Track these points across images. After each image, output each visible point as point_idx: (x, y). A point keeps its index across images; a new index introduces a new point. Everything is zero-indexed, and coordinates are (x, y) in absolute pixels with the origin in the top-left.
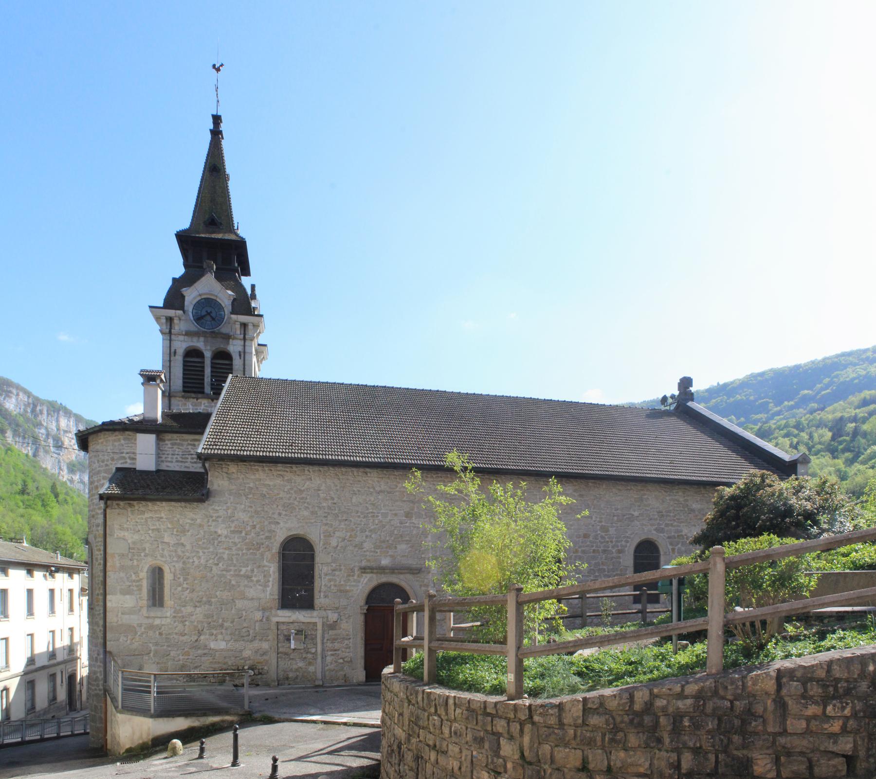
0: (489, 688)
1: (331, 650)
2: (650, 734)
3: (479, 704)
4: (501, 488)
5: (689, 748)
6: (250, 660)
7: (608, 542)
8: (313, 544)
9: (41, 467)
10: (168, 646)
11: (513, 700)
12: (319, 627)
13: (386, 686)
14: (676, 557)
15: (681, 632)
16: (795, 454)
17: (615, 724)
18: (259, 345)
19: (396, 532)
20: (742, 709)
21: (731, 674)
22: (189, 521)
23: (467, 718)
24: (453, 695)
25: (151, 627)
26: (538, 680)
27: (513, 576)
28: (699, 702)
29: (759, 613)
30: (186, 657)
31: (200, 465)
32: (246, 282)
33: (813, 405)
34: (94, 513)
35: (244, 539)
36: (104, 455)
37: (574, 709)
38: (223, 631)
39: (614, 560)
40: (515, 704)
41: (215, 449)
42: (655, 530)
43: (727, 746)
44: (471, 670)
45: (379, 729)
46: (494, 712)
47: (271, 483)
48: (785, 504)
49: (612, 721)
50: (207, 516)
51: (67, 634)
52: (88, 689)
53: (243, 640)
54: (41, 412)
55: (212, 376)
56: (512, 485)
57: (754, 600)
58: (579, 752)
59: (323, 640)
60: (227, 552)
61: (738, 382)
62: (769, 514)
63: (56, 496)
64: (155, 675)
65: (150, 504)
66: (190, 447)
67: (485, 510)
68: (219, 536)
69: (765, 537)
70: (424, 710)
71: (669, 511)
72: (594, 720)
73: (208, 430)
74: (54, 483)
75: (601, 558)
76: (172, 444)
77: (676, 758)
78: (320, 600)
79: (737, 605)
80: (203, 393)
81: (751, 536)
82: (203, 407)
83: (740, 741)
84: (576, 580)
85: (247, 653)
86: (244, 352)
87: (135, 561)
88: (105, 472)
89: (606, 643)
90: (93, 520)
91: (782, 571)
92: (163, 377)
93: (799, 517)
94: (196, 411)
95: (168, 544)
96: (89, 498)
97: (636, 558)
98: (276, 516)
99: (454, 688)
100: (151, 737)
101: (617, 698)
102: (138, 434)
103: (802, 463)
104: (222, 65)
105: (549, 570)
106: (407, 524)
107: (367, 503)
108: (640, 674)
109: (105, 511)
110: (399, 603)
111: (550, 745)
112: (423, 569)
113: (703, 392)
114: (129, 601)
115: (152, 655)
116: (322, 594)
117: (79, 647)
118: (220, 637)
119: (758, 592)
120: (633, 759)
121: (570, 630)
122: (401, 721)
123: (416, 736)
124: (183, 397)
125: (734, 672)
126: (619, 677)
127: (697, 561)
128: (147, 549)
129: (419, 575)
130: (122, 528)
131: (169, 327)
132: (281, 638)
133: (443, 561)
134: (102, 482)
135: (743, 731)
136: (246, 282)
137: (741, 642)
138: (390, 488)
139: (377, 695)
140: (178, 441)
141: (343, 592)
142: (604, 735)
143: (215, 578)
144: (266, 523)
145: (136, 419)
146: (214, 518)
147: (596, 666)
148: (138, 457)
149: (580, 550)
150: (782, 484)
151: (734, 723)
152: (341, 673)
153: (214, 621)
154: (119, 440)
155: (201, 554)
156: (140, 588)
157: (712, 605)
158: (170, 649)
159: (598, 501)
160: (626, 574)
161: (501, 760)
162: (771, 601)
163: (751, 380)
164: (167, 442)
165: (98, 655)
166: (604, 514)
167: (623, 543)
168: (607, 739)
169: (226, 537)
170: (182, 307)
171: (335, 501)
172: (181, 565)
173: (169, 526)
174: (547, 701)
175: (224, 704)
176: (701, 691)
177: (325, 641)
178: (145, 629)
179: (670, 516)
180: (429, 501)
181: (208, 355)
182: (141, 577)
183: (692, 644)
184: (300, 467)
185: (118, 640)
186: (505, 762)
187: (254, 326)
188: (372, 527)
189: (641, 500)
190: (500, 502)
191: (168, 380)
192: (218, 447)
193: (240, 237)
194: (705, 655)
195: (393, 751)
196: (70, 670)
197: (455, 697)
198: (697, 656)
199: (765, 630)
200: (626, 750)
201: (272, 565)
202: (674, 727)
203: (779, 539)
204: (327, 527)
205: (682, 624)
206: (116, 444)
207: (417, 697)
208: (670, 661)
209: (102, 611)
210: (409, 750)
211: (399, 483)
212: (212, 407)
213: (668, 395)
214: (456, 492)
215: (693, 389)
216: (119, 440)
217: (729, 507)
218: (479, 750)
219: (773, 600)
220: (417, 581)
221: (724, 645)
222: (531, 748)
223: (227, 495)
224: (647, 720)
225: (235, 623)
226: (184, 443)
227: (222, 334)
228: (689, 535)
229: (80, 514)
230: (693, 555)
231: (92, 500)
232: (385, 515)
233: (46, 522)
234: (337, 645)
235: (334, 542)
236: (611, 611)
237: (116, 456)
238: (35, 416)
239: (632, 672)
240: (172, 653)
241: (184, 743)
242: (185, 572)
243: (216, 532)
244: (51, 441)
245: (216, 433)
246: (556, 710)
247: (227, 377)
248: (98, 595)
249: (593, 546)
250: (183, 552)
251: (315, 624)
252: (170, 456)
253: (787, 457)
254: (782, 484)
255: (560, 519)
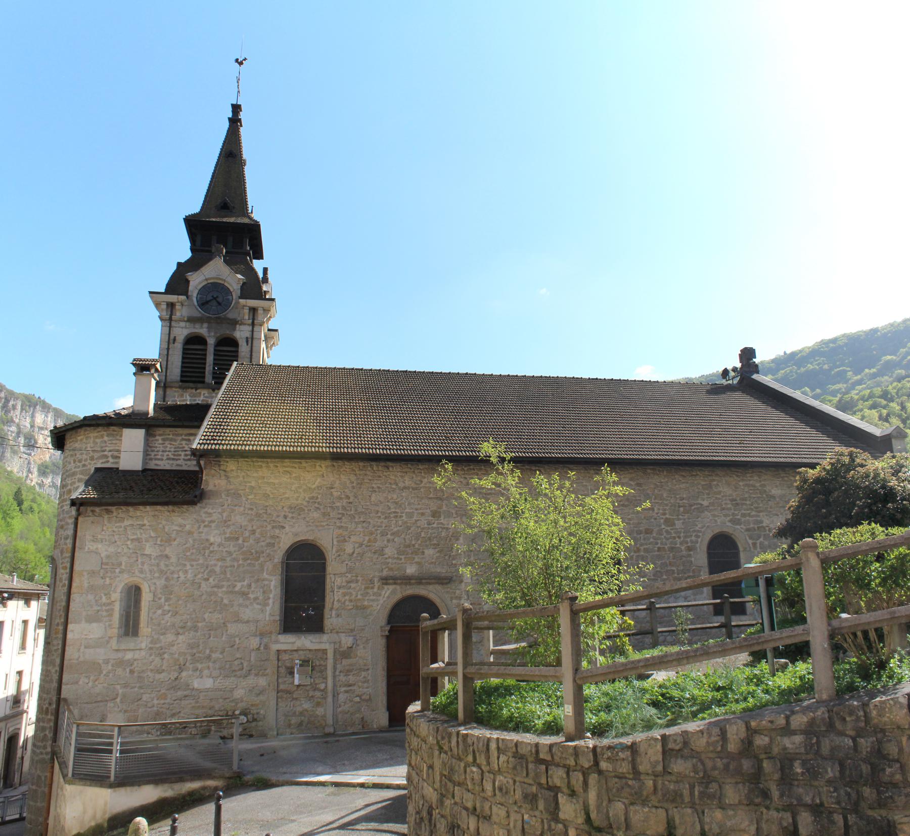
0: (541, 725)
1: (346, 686)
2: (752, 786)
3: (529, 748)
4: (545, 480)
5: (806, 805)
6: (242, 701)
7: (674, 538)
8: (324, 551)
9: (6, 471)
10: (141, 688)
11: (572, 740)
12: (330, 655)
13: (412, 730)
14: (759, 553)
15: (776, 645)
16: (887, 428)
17: (705, 772)
18: (269, 330)
19: (423, 535)
20: (869, 749)
21: (848, 700)
22: (177, 528)
23: (514, 768)
24: (495, 736)
25: (121, 663)
26: (602, 713)
27: (564, 583)
28: (811, 739)
29: (872, 619)
30: (162, 702)
31: (195, 463)
32: (258, 265)
33: (900, 371)
34: (63, 523)
35: (241, 548)
36: (82, 454)
37: (650, 752)
38: (211, 664)
39: (684, 559)
40: (575, 747)
41: (212, 444)
42: (730, 521)
43: (856, 804)
44: (517, 703)
45: (405, 792)
46: (549, 758)
47: (277, 481)
48: (884, 487)
49: (701, 767)
50: (197, 521)
51: (13, 679)
52: (33, 752)
53: (235, 676)
54: (14, 407)
55: (215, 364)
56: (558, 476)
57: (863, 604)
58: (662, 813)
59: (335, 671)
60: (220, 563)
61: (807, 351)
62: (866, 498)
63: (20, 503)
64: (120, 727)
65: (131, 509)
66: (184, 442)
67: (528, 506)
68: (211, 544)
69: (864, 527)
70: (460, 759)
71: (745, 499)
72: (679, 766)
73: (205, 423)
74: (19, 488)
75: (669, 558)
76: (163, 440)
77: (790, 820)
78: (331, 620)
79: (843, 611)
80: (203, 382)
81: (848, 526)
82: (202, 398)
83: (874, 796)
84: (640, 585)
85: (239, 693)
86: (252, 338)
87: (108, 579)
88: (82, 473)
89: (685, 661)
90: (61, 532)
91: (892, 566)
92: (158, 366)
93: (904, 502)
94: (194, 403)
95: (149, 556)
96: (59, 504)
97: (710, 555)
98: (281, 519)
99: (496, 728)
100: (107, 816)
101: (705, 734)
102: (124, 430)
103: (896, 438)
104: (245, 59)
105: (608, 573)
106: (435, 525)
107: (388, 501)
108: (732, 702)
109: (77, 519)
110: (425, 619)
111: (624, 803)
112: (455, 578)
113: (768, 363)
114: (95, 631)
115: (118, 700)
116: (334, 612)
117: (27, 698)
118: (206, 672)
119: (867, 594)
120: (734, 822)
121: (638, 650)
122: (431, 776)
123: (450, 796)
124: (180, 387)
125: (852, 697)
126: (705, 707)
127: (785, 558)
128: (124, 564)
129: (449, 585)
130: (95, 540)
131: (169, 313)
132: (282, 670)
133: (480, 567)
134: (77, 484)
135: (875, 780)
136: (258, 265)
137: (855, 660)
138: (415, 483)
139: (401, 744)
140: (171, 436)
141: (361, 609)
142: (692, 788)
143: (204, 597)
144: (269, 527)
145: (124, 412)
146: (206, 523)
147: (676, 693)
148: (122, 455)
149: (642, 548)
150: (876, 463)
151: (861, 770)
152: (357, 715)
153: (200, 653)
154: (102, 436)
155: (188, 567)
156: (110, 613)
157: (811, 609)
158: (142, 691)
159: (660, 491)
160: (701, 576)
161: (560, 826)
162: (885, 604)
163: (823, 348)
164: (157, 437)
165: (50, 704)
166: (667, 505)
167: (693, 538)
168: (696, 793)
169: (219, 545)
170: (185, 292)
171: (351, 500)
172: (163, 582)
173: (153, 534)
174: (617, 741)
175: (208, 764)
176: (812, 723)
177: (337, 673)
178: (113, 666)
179: (746, 504)
180: (461, 498)
181: (211, 341)
182: (113, 599)
183: (793, 662)
184: (311, 462)
185: (77, 683)
186: (566, 827)
187: (264, 310)
188: (395, 529)
189: (710, 487)
190: (546, 495)
191: (164, 370)
192: (216, 442)
193: (254, 220)
194: (810, 676)
195: (422, 819)
196: (11, 729)
197: (498, 739)
198: (801, 678)
199: (883, 643)
200: (723, 808)
201: (273, 578)
202: (782, 774)
203: (884, 529)
204: (341, 530)
205: (777, 634)
206: (98, 441)
207: (450, 742)
208: (767, 685)
209: (60, 647)
210: (442, 816)
211: (425, 478)
212: (212, 397)
213: (730, 368)
214: (493, 486)
215: (757, 360)
216: (102, 436)
217: (815, 492)
218: (531, 812)
219: (888, 603)
220: (448, 592)
221: (833, 663)
222: (599, 807)
223: (223, 496)
224: (747, 765)
225: (225, 654)
226: (177, 438)
227: (229, 319)
228: (772, 526)
229: (48, 526)
230: (779, 550)
231: (61, 507)
232: (410, 515)
233: (4, 538)
234: (352, 679)
235: (349, 548)
236: (688, 625)
237: (96, 455)
238: (6, 411)
239: (720, 701)
240: (145, 698)
241: (151, 822)
242: (167, 590)
243: (207, 540)
244: (22, 440)
245: (216, 426)
246: (629, 753)
247: (231, 365)
248: (58, 624)
249: (657, 544)
250: (167, 566)
251: (324, 651)
252: (160, 453)
253: (877, 432)
254: (876, 463)
255: (616, 512)
